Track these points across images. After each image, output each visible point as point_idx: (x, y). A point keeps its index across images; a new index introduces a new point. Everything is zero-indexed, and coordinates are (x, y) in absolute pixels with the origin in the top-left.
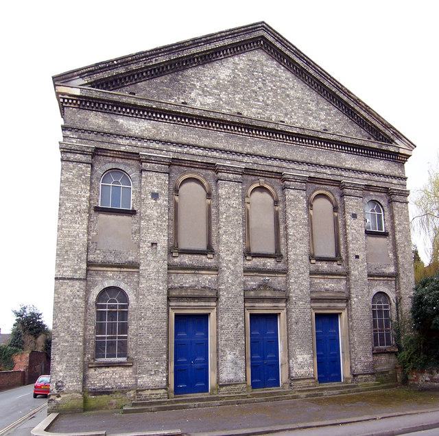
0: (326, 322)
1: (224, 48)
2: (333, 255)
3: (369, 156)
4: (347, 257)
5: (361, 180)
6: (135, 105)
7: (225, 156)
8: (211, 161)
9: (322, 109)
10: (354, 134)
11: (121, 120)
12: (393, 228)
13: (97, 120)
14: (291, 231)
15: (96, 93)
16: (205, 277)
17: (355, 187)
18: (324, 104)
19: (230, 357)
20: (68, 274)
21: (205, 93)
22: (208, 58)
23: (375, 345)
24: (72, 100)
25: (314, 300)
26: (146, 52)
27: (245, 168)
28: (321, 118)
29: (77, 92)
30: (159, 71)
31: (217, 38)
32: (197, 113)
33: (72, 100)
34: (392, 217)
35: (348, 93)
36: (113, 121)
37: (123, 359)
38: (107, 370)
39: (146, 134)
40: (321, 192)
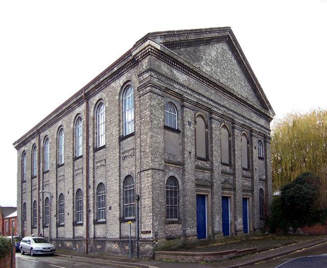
0: (201, 199)
1: (215, 38)
2: (205, 157)
3: (260, 116)
4: (253, 169)
5: (194, 98)
6: (183, 64)
7: (214, 105)
8: (210, 107)
9: (246, 86)
10: (257, 105)
11: (175, 72)
12: (266, 155)
13: (164, 68)
14: (236, 153)
15: (167, 51)
16: (206, 174)
17: (191, 102)
18: (247, 84)
19: (217, 219)
20: (157, 167)
21: (207, 64)
22: (208, 42)
23: (168, 218)
24: (155, 51)
25: (244, 191)
26: (188, 30)
27: (197, 102)
28: (244, 91)
29: (159, 47)
30: (189, 44)
31: (213, 31)
32: (207, 76)
33: (159, 54)
34: (266, 150)
35: (256, 80)
36: (171, 71)
37: (176, 219)
38: (172, 225)
39: (185, 84)
40: (202, 114)
